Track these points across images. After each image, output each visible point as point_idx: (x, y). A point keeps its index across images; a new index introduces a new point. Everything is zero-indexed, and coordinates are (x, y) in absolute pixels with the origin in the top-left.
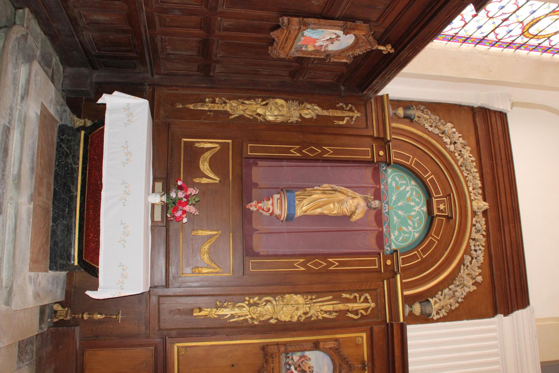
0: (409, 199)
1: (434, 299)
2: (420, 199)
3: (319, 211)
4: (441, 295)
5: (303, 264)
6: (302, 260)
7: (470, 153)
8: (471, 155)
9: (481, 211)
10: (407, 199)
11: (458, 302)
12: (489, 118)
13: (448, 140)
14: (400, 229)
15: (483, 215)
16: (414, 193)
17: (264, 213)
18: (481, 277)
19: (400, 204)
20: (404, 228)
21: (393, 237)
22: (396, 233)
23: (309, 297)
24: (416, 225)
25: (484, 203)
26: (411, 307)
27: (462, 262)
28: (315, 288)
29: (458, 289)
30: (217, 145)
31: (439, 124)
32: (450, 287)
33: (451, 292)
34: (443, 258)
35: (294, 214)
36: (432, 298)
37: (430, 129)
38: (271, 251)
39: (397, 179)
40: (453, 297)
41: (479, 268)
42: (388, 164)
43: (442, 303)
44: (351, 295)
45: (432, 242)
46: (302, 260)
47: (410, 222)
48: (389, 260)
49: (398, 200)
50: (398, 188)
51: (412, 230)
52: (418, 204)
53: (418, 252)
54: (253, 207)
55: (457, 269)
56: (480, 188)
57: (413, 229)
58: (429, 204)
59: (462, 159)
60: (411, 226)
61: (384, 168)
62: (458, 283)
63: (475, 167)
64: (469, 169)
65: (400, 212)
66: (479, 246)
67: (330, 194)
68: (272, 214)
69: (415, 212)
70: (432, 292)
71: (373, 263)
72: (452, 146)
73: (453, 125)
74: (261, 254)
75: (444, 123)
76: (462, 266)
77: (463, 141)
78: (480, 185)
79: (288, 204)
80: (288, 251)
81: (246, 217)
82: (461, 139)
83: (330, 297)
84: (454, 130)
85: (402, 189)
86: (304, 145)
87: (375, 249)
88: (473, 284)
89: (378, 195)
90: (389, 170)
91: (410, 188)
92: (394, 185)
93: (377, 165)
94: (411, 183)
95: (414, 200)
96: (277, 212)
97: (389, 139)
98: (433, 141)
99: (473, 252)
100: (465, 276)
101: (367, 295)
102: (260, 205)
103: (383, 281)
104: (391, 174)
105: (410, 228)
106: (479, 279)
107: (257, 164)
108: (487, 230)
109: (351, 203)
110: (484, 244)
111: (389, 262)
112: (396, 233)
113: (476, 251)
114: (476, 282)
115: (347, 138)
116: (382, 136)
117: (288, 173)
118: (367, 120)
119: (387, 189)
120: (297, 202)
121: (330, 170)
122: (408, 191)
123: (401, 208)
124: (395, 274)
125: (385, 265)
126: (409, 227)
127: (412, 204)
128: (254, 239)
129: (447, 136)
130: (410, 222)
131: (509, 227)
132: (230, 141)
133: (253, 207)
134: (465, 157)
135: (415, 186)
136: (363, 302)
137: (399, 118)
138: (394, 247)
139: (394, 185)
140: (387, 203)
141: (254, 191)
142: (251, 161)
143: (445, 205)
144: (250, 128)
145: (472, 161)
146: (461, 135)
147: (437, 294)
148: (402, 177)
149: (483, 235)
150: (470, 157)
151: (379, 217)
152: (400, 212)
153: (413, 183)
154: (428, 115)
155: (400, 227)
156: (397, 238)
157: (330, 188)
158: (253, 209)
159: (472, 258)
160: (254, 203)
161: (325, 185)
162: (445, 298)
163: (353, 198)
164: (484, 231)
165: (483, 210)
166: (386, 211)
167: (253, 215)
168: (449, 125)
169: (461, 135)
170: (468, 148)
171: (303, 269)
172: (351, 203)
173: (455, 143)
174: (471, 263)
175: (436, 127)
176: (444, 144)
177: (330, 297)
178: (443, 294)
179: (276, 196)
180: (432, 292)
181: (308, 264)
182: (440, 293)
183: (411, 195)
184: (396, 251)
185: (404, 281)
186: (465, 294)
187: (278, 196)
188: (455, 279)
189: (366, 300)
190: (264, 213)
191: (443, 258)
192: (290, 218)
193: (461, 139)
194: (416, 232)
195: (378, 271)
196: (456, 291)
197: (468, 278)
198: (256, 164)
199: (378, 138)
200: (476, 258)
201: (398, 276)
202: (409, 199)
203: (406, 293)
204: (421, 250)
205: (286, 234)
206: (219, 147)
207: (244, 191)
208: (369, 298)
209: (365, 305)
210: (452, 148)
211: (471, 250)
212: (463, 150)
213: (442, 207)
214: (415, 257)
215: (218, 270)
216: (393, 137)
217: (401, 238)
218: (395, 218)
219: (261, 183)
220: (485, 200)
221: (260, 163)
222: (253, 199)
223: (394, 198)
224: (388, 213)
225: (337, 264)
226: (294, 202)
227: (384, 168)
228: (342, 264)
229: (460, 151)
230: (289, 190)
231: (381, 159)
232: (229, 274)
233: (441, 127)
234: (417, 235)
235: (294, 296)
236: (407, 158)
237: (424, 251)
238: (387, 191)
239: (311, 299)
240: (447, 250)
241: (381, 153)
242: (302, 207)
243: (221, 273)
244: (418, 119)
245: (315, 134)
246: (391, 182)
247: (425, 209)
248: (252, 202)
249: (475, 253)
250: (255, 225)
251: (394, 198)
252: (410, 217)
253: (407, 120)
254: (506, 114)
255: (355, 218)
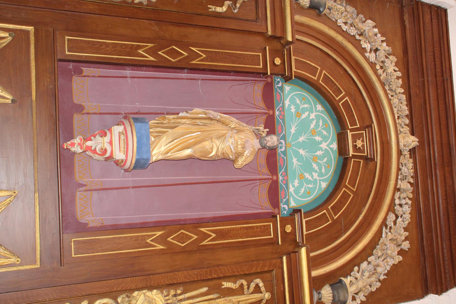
0: (314, 132)
1: (349, 278)
2: (329, 132)
3: (188, 152)
4: (358, 272)
5: (162, 240)
6: (159, 233)
7: (396, 66)
8: (397, 69)
9: (408, 149)
10: (311, 131)
11: (379, 281)
12: (421, 15)
13: (367, 46)
14: (302, 177)
15: (410, 154)
16: (321, 123)
17: (96, 157)
18: (408, 242)
19: (301, 139)
20: (307, 175)
21: (291, 189)
22: (296, 183)
23: (172, 292)
24: (323, 171)
25: (413, 138)
26: (319, 293)
27: (384, 223)
28: (181, 276)
29: (380, 261)
30: (6, 35)
31: (357, 20)
32: (370, 259)
33: (371, 267)
34: (361, 218)
35: (148, 159)
36: (346, 277)
37: (345, 28)
38: (109, 220)
39: (298, 102)
40: (373, 274)
41: (406, 229)
42: (287, 79)
43: (360, 284)
44: (235, 282)
45: (345, 196)
46: (159, 233)
47: (314, 165)
48: (289, 226)
49: (299, 133)
50: (298, 115)
51: (318, 178)
52: (325, 139)
53: (328, 210)
54: (76, 145)
55: (379, 234)
56: (407, 116)
57: (318, 176)
58: (341, 139)
59: (385, 74)
60: (316, 172)
61: (280, 85)
62: (380, 254)
63: (402, 87)
64: (393, 89)
65: (302, 152)
66: (405, 199)
67: (205, 125)
68: (111, 157)
69: (322, 150)
70: (346, 269)
71: (266, 230)
72: (373, 54)
73: (374, 24)
74: (91, 225)
75: (364, 19)
76: (384, 228)
77: (387, 48)
78: (407, 112)
79: (138, 142)
80: (137, 218)
81: (64, 162)
82: (384, 44)
83: (205, 289)
84: (376, 30)
85: (304, 116)
86: (161, 43)
87: (267, 208)
88: (399, 253)
89: (271, 126)
90: (287, 88)
91: (315, 116)
92: (293, 110)
93: (269, 80)
94: (316, 108)
95: (320, 134)
96: (119, 155)
97: (290, 39)
98: (350, 47)
99: (397, 207)
100: (388, 243)
101: (258, 281)
102: (89, 143)
103: (282, 258)
104: (289, 93)
105: (315, 175)
106: (406, 245)
107: (81, 72)
108: (415, 177)
109: (237, 141)
110: (411, 196)
111: (289, 229)
112: (296, 183)
113: (401, 205)
114: (401, 250)
115: (228, 34)
116: (278, 35)
117: (133, 88)
118: (257, 7)
119: (284, 115)
120: (153, 139)
121: (201, 84)
122: (313, 119)
123: (302, 145)
124: (298, 246)
125: (284, 232)
126: (314, 174)
127: (318, 138)
128: (93, 226)
129: (366, 38)
130: (314, 165)
131: (444, 170)
132: (31, 28)
133: (76, 145)
134: (389, 71)
135: (322, 112)
136: (252, 293)
137: (302, 8)
138: (293, 204)
139: (293, 110)
140: (284, 138)
141: (77, 118)
142: (71, 66)
143: (363, 141)
144: (67, 7)
145: (398, 78)
146: (384, 39)
147: (352, 270)
148: (304, 99)
149: (409, 182)
150: (395, 71)
151: (272, 159)
152: (302, 152)
153: (319, 107)
154: (343, 6)
155: (302, 174)
156: (297, 191)
157: (204, 116)
158: (77, 149)
159: (397, 217)
160: (77, 140)
161: (196, 110)
162: (363, 275)
163: (239, 131)
164: (412, 177)
165: (411, 147)
166: (283, 149)
167: (76, 158)
168: (370, 23)
169: (384, 39)
170: (392, 58)
171: (162, 247)
172: (237, 141)
173: (376, 50)
174: (395, 223)
175: (351, 25)
176: (362, 51)
177: (205, 289)
178: (361, 271)
179: (117, 129)
180: (346, 269)
181: (169, 239)
182: (356, 268)
183: (317, 125)
184: (297, 211)
185: (312, 254)
186: (388, 268)
187: (120, 128)
188: (375, 248)
189: (257, 290)
190: (96, 157)
191: (361, 218)
192: (141, 164)
193: (384, 44)
194: (323, 181)
195: (274, 242)
196: (378, 266)
197: (392, 245)
198: (79, 72)
199: (273, 37)
200: (401, 216)
201: (303, 251)
202: (314, 132)
203: (315, 273)
204: (331, 208)
205: (132, 190)
206: (10, 39)
207: (59, 120)
208: (261, 284)
209: (257, 296)
210: (372, 57)
211: (395, 205)
212: (386, 60)
213: (359, 144)
214: (323, 218)
215: (13, 260)
216: (298, 37)
217: (303, 190)
218: (295, 160)
219: (89, 106)
220: (413, 134)
221: (87, 70)
222: (75, 132)
223: (293, 130)
224: (285, 153)
225: (214, 235)
226: (148, 138)
227: (280, 85)
228: (221, 235)
229: (383, 62)
230: (137, 117)
231: (277, 70)
232: (34, 267)
233: (360, 25)
234: (324, 185)
235: (149, 293)
236: (313, 71)
237: (336, 209)
238: (283, 120)
239: (175, 295)
240: (364, 206)
241: (278, 61)
242: (161, 147)
243: (19, 265)
244: (328, 11)
245: (178, 24)
246: (289, 106)
247: (335, 146)
248: (72, 137)
249: (400, 209)
250: (79, 177)
251: (293, 130)
252: (315, 159)
253: (313, 12)
254: (445, 11)
255: (241, 162)
